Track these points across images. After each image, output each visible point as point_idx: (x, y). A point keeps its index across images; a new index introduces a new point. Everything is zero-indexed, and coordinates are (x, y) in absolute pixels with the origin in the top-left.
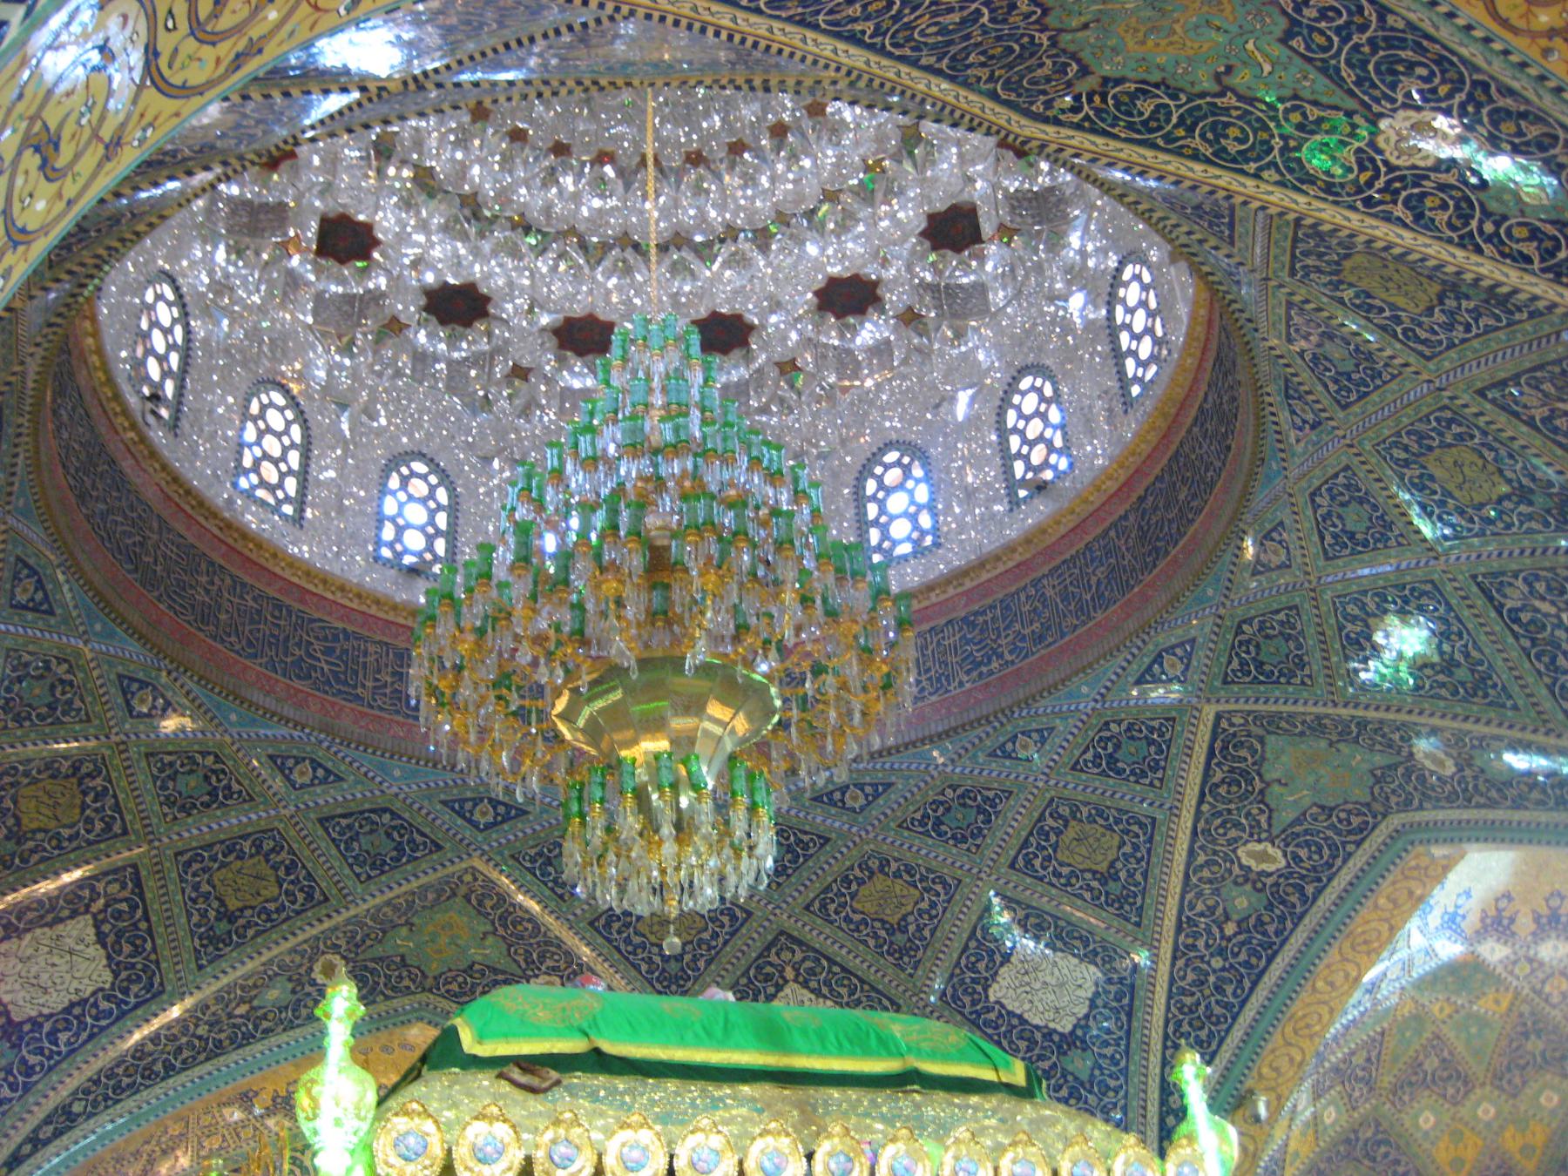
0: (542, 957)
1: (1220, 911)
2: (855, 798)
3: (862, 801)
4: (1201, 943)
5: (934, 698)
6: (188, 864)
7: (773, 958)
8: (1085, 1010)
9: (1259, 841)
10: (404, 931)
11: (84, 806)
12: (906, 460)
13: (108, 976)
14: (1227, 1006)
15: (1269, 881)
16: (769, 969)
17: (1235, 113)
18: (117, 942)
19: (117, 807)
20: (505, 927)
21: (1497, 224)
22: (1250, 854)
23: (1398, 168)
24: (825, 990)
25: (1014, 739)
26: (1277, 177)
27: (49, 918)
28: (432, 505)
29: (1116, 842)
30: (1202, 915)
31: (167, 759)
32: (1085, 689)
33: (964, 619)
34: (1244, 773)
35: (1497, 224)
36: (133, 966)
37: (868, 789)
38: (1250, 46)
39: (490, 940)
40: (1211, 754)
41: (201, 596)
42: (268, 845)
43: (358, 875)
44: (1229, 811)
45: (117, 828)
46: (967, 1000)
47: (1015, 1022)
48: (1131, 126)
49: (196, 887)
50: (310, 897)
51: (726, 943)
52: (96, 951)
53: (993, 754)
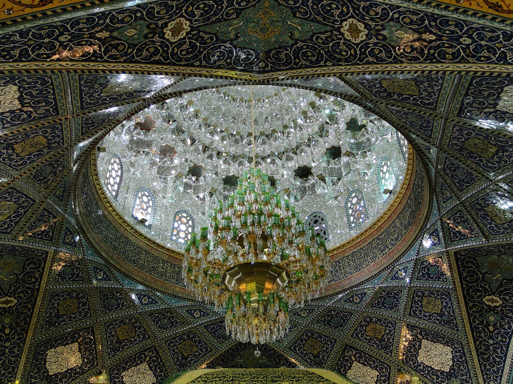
1: (485, 322)
2: (356, 299)
3: (359, 300)
4: (482, 335)
5: (372, 264)
6: (169, 344)
7: (347, 354)
8: (452, 363)
9: (490, 295)
10: (239, 357)
11: (136, 332)
13: (155, 379)
14: (500, 357)
15: (499, 309)
16: (346, 358)
17: (305, 47)
18: (155, 369)
19: (145, 330)
21: (136, 16)
23: (349, 17)
24: (366, 363)
26: (331, 64)
27: (135, 364)
28: (187, 232)
29: (440, 302)
30: (478, 324)
31: (156, 315)
32: (412, 253)
34: (473, 272)
35: (136, 16)
36: (161, 375)
37: (360, 296)
38: (289, 23)
40: (459, 268)
41: (160, 270)
42: (191, 336)
43: (219, 342)
44: (474, 286)
45: (147, 336)
46: (411, 362)
47: (429, 369)
48: (284, 65)
49: (174, 351)
50: (207, 350)
51: (331, 350)
52: (150, 372)
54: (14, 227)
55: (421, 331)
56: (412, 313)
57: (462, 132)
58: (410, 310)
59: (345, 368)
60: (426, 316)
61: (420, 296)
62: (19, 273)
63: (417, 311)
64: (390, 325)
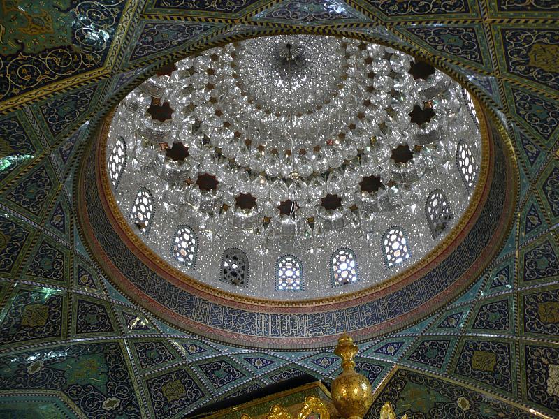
0: (119, 389)
2: (259, 363)
12: (397, 232)
16: (534, 363)
20: (113, 372)
22: (114, 402)
25: (322, 359)
26: (18, 91)
33: (311, 315)
37: (265, 361)
39: (103, 375)
53: (439, 326)
54: (14, 263)
55: (545, 352)
56: (529, 329)
57: (518, 40)
58: (525, 324)
59: (541, 377)
60: (547, 329)
61: (470, 349)
62: (106, 371)
63: (533, 324)
64: (502, 350)
